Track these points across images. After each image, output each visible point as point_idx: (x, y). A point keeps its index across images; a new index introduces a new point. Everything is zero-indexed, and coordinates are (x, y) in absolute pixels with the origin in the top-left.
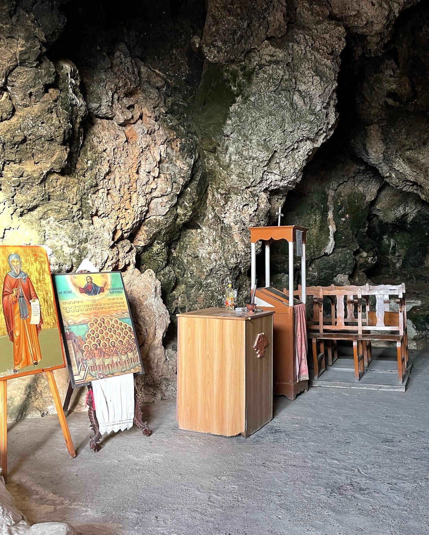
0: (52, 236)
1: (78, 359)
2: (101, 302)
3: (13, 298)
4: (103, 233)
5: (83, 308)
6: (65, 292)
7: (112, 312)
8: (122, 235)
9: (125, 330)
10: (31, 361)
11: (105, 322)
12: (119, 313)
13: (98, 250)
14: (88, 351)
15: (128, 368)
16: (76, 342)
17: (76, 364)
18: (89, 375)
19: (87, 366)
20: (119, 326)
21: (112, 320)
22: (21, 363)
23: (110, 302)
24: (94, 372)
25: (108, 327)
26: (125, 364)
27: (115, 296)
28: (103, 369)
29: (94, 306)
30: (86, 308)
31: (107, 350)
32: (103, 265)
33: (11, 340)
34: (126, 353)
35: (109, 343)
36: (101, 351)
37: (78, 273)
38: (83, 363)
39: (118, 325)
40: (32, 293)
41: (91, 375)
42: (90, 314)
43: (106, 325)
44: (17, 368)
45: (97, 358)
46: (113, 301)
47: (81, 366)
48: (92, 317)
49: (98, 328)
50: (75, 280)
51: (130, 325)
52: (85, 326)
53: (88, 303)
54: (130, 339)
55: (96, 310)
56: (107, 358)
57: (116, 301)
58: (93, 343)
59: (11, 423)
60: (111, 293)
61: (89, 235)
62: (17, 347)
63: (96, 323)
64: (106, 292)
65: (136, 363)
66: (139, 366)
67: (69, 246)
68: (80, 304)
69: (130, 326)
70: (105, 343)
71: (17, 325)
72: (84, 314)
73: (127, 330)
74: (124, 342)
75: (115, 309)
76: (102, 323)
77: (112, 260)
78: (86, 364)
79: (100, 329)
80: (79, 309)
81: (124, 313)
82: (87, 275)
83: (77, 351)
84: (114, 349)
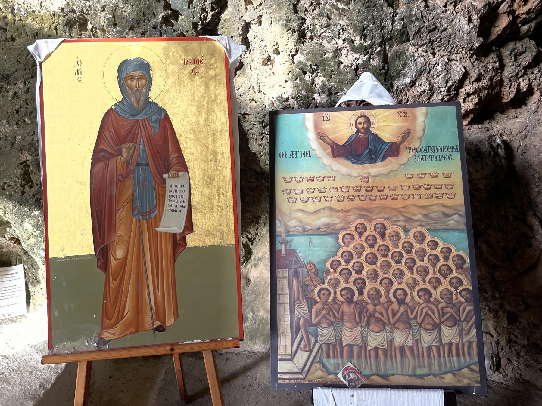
0: (319, 30)
1: (295, 320)
2: (387, 182)
3: (120, 167)
4: (451, 17)
5: (331, 194)
6: (294, 154)
7: (413, 209)
8: (513, 24)
9: (442, 262)
10: (148, 321)
11: (387, 235)
12: (433, 215)
13: (440, 58)
14: (326, 303)
15: (436, 369)
16: (300, 275)
17: (289, 330)
18: (318, 365)
19: (316, 341)
20: (428, 249)
21: (407, 231)
22: (119, 326)
23: (412, 182)
24: (332, 361)
25: (392, 249)
26: (429, 356)
27: (429, 167)
28: (359, 356)
29: (363, 192)
30: (340, 193)
31: (379, 308)
32: (453, 93)
33: (100, 267)
34: (436, 326)
35: (388, 292)
36: (361, 307)
37: (340, 107)
38: (307, 332)
39: (425, 246)
40: (173, 156)
41: (324, 366)
42: (348, 211)
43: (389, 243)
44: (107, 335)
45: (349, 325)
46: (421, 182)
47: (302, 339)
48: (353, 217)
49: (363, 248)
50: (327, 126)
51: (464, 251)
52: (329, 240)
53: (346, 183)
54: (456, 288)
55: (368, 200)
56: (376, 329)
57: (428, 180)
58: (343, 285)
59: (263, 352)
60: (417, 159)
61: (411, 22)
62: (113, 284)
63: (360, 235)
64: (405, 156)
65: (465, 360)
66: (472, 370)
67: (355, 50)
68: (326, 183)
69: (461, 253)
70: (378, 291)
71: (121, 231)
72: (331, 208)
73: (450, 263)
74: (436, 294)
75: (423, 202)
76: (378, 237)
77: (478, 80)
78: (315, 335)
79: (368, 250)
80: (323, 195)
81: (447, 215)
82: (358, 113)
83: (298, 299)
84: (402, 309)
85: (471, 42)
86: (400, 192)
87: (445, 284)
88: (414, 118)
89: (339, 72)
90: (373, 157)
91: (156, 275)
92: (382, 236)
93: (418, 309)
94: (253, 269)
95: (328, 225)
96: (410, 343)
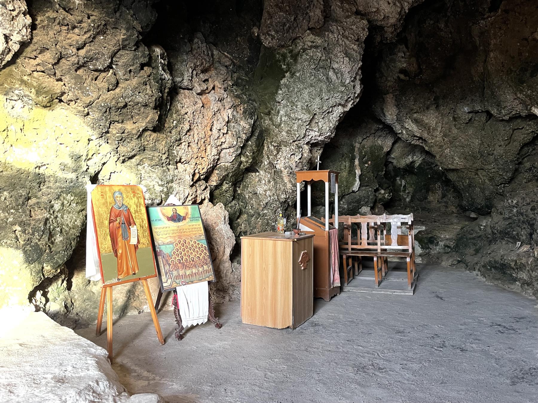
2: (184, 227)
6: (156, 220)
7: (192, 235)
8: (199, 177)
9: (201, 249)
10: (131, 272)
15: (204, 277)
21: (191, 241)
24: (178, 280)
27: (194, 223)
28: (185, 278)
30: (172, 232)
33: (115, 256)
34: (202, 266)
36: (183, 264)
40: (131, 220)
43: (187, 245)
46: (193, 227)
50: (164, 211)
52: (171, 246)
53: (173, 228)
57: (194, 226)
58: (177, 258)
62: (120, 261)
63: (180, 243)
64: (188, 220)
67: (159, 185)
68: (167, 229)
72: (170, 236)
73: (203, 249)
74: (201, 257)
77: (192, 196)
78: (172, 274)
79: (182, 248)
81: (200, 236)
82: (173, 207)
85: (190, 183)
86: (188, 230)
87: (203, 254)
88: (188, 209)
89: (155, 193)
90: (179, 220)
91: (131, 257)
92: (185, 243)
93: (197, 262)
94: (94, 286)
95: (170, 242)
96: (197, 272)
